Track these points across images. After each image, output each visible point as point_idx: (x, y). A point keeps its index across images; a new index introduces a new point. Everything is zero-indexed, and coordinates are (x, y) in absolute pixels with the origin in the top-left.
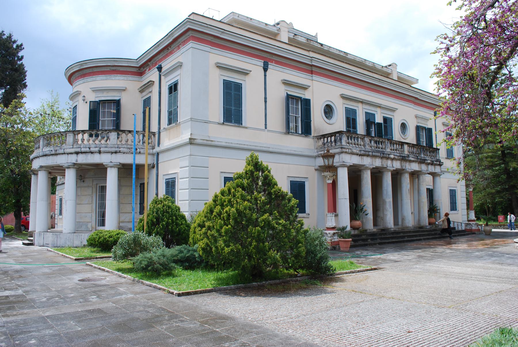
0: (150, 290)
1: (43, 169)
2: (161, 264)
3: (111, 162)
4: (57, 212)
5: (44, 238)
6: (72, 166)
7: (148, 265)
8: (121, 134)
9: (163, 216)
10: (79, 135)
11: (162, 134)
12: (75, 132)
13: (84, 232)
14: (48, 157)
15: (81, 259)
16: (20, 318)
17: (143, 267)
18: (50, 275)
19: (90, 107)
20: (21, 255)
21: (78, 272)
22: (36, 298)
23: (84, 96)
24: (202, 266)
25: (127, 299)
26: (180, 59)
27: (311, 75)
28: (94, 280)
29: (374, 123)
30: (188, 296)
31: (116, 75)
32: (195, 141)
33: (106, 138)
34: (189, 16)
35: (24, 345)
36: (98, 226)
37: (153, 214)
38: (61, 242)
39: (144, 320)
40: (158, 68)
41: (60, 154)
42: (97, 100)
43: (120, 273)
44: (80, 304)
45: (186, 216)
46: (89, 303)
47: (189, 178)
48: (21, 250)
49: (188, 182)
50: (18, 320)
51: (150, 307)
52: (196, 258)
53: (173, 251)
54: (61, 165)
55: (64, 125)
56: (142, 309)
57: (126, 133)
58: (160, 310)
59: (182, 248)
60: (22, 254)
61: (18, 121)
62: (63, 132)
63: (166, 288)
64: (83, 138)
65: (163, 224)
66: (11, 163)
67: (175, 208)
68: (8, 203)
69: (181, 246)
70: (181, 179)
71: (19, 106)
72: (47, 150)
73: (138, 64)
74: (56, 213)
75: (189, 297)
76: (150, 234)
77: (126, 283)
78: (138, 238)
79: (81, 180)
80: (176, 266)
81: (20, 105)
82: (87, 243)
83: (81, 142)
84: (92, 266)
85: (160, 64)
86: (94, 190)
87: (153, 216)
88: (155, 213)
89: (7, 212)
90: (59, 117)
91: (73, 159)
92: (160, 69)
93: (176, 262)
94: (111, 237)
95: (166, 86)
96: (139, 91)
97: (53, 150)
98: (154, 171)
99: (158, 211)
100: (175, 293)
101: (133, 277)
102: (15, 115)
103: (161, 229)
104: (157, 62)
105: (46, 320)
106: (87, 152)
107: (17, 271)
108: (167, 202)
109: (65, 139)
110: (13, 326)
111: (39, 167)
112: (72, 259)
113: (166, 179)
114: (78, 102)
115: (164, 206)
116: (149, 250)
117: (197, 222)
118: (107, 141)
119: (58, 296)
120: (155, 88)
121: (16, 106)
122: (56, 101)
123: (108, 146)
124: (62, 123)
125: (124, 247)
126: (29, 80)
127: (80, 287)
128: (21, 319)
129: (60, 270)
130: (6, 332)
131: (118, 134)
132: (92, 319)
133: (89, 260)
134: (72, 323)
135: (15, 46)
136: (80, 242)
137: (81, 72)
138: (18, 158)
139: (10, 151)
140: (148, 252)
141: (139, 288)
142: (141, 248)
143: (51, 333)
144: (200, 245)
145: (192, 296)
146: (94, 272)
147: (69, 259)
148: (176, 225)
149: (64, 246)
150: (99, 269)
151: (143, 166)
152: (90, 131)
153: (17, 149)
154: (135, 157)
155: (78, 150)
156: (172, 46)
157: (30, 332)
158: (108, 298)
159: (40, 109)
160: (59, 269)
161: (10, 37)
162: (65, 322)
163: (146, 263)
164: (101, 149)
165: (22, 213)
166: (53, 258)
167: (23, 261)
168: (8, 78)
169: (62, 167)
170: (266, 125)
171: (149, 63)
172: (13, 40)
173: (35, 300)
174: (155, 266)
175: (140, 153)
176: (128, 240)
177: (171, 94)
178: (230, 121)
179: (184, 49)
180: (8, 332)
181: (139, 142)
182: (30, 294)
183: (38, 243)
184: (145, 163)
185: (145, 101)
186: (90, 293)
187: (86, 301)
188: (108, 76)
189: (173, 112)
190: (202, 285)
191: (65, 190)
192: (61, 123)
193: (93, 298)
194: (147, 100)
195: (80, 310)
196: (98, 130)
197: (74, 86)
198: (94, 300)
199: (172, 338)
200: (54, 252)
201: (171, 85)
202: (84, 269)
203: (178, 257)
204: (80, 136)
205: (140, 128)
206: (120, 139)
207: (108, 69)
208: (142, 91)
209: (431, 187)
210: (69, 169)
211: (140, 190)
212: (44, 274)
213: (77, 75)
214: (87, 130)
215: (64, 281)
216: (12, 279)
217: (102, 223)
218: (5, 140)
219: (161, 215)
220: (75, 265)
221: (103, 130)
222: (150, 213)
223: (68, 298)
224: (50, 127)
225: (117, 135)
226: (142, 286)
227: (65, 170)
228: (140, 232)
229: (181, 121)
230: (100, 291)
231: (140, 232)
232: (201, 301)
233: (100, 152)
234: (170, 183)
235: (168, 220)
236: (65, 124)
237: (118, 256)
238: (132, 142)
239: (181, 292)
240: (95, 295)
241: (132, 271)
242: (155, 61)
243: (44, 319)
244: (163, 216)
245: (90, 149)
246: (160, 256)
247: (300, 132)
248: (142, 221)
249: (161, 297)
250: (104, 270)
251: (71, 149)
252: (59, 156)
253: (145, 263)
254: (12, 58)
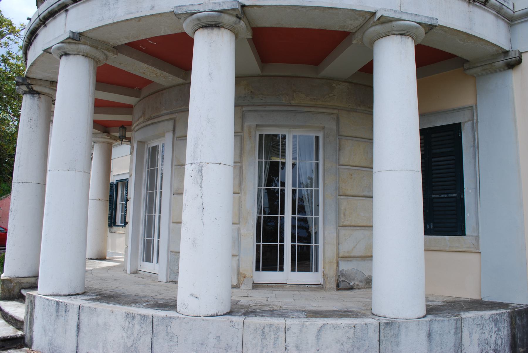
5: (83, 328)
183: (51, 344)
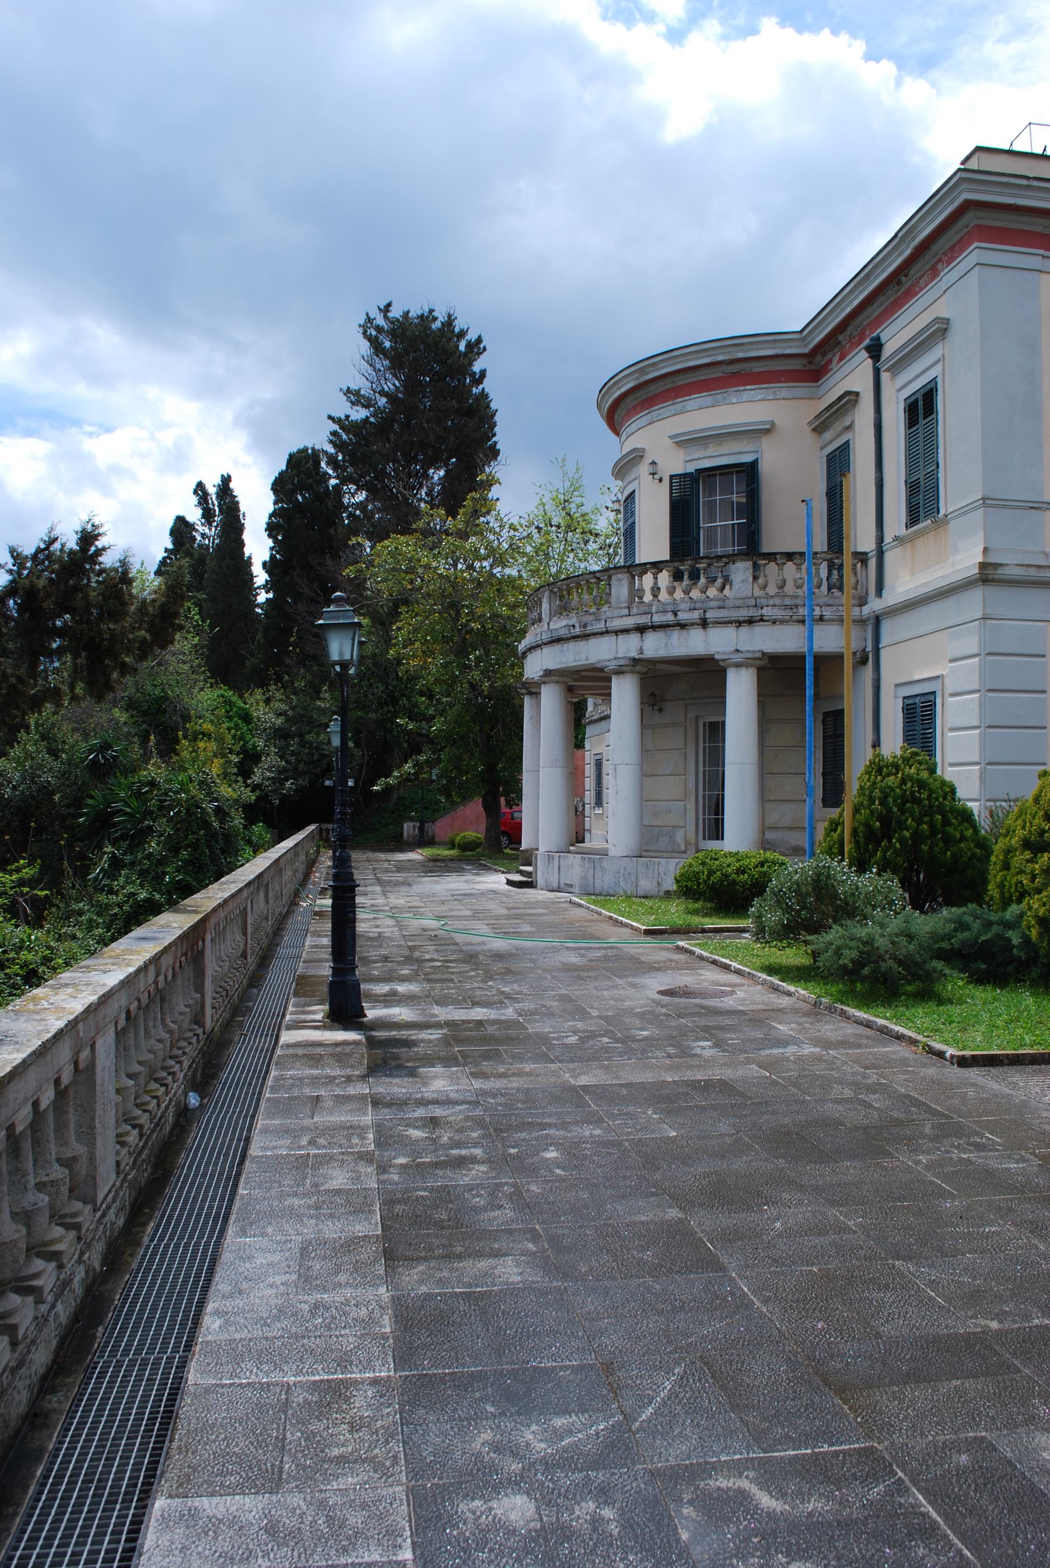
0: (868, 1038)
1: (553, 678)
2: (900, 963)
3: (737, 651)
4: (589, 797)
6: (630, 668)
7: (860, 962)
8: (765, 565)
9: (902, 811)
10: (644, 577)
11: (889, 557)
12: (634, 569)
13: (665, 855)
14: (566, 645)
15: (661, 932)
16: (515, 1083)
17: (844, 966)
18: (584, 970)
19: (671, 493)
20: (504, 912)
21: (658, 969)
22: (550, 1033)
23: (654, 463)
24: (1034, 975)
25: (801, 1059)
26: (942, 310)
28: (703, 994)
30: (991, 1069)
31: (742, 388)
32: (999, 572)
33: (720, 581)
34: (963, 163)
35: (529, 1161)
36: (704, 839)
37: (869, 806)
38: (604, 881)
39: (857, 1128)
40: (868, 349)
41: (595, 634)
42: (691, 468)
43: (775, 980)
44: (667, 1061)
45: (976, 812)
46: (694, 1062)
47: (978, 691)
48: (505, 900)
49: (976, 705)
50: (511, 1089)
51: (875, 1092)
52: (1013, 947)
53: (935, 922)
54: (598, 666)
55: (600, 552)
56: (848, 1093)
57: (780, 561)
58: (904, 1103)
59: (965, 913)
60: (509, 909)
61: (482, 551)
62: (599, 571)
63: (920, 1038)
64: (656, 583)
65: (904, 836)
66: (469, 667)
67: (941, 788)
68: (467, 773)
69: (964, 909)
70: (952, 695)
71: (484, 510)
72: (560, 625)
73: (806, 346)
74: (587, 800)
75: (994, 1071)
76: (862, 867)
77: (796, 1011)
78: (828, 877)
79: (653, 705)
80: (947, 971)
81: (484, 506)
82: (675, 887)
83: (651, 598)
84: (692, 953)
85: (875, 334)
86: (691, 734)
87: (872, 812)
88: (877, 802)
89: (465, 798)
90: (586, 530)
91: (629, 647)
92: (875, 350)
93: (947, 956)
94: (744, 872)
95: (897, 403)
96: (814, 430)
97: (577, 625)
98: (868, 671)
99: (886, 796)
100: (948, 1055)
101: (815, 994)
102: (475, 534)
103: (896, 852)
104: (865, 329)
105: (583, 1097)
106: (669, 626)
107: (499, 956)
108: (913, 770)
109: (607, 590)
110: (500, 1105)
111: (541, 673)
112: (636, 929)
113: (904, 698)
114: (636, 482)
115: (903, 781)
116: (861, 915)
117: (1020, 833)
118: (722, 589)
119: (608, 1033)
120: (863, 416)
121: (476, 511)
122: (576, 487)
123: (727, 603)
124: (595, 546)
125: (787, 904)
126: (502, 437)
127: (664, 1010)
128: (518, 1089)
129: (606, 958)
130: (484, 1120)
131: (756, 567)
132: (703, 1108)
133: (683, 936)
134: (650, 1113)
135: (462, 347)
136: (655, 883)
137: (640, 393)
138: (487, 652)
139: (467, 633)
140: (858, 922)
141: (831, 1029)
142: (837, 909)
143: (598, 1136)
144: (1030, 908)
145: (1006, 1068)
146: (700, 971)
147: (628, 930)
148: (944, 842)
149: (612, 892)
150: (714, 962)
151: (837, 659)
152: (676, 564)
153: (483, 627)
154: (811, 632)
155: (644, 620)
156: (911, 273)
157: (543, 1126)
158: (746, 1052)
159: (536, 512)
160: (605, 956)
161: (450, 322)
162: (631, 1109)
163: (855, 954)
164: (708, 615)
165: (502, 800)
166: (585, 924)
167: (511, 930)
168: (452, 438)
169: (601, 670)
171: (841, 337)
172: (457, 330)
173: (548, 1038)
174: (883, 964)
175: (821, 619)
176: (797, 883)
177: (916, 427)
179: (955, 274)
180: (488, 1119)
181: (819, 586)
182: (537, 1021)
184: (844, 650)
185: (831, 459)
186: (692, 1031)
187: (685, 1052)
188: (719, 395)
189: (922, 484)
190: (1037, 1035)
191: (611, 737)
192: (592, 546)
193: (703, 1048)
194: (837, 453)
195: (670, 1079)
196: (698, 559)
197: (624, 437)
198: (708, 1053)
199: (953, 1197)
200: (588, 908)
201: (912, 399)
202: (671, 961)
203: (953, 941)
204: (648, 580)
205: (820, 543)
206: (761, 580)
207: (716, 373)
208: (820, 426)
210: (621, 676)
211: (824, 733)
212: (568, 968)
213: (629, 401)
214: (666, 561)
215: (621, 992)
216: (489, 976)
217: (716, 830)
218: (455, 605)
219: (895, 809)
220: (646, 948)
221: (712, 558)
222: (861, 804)
223: (635, 1040)
224: (563, 561)
225: (751, 570)
226: (843, 1024)
227: (609, 680)
228: (833, 859)
229: (950, 510)
230: (720, 1028)
231: (833, 859)
232: (1037, 1089)
233: (704, 623)
234: (919, 710)
235: (919, 822)
236: (601, 548)
237: (770, 928)
238: (798, 587)
239: (968, 1053)
240: (707, 1040)
241: (809, 975)
242: (859, 329)
243: (574, 1094)
244: (903, 811)
245: (676, 615)
246: (897, 935)
248: (837, 824)
249: (905, 1062)
250: (726, 968)
251: (625, 618)
252: (593, 641)
253: (853, 956)
254: (459, 380)
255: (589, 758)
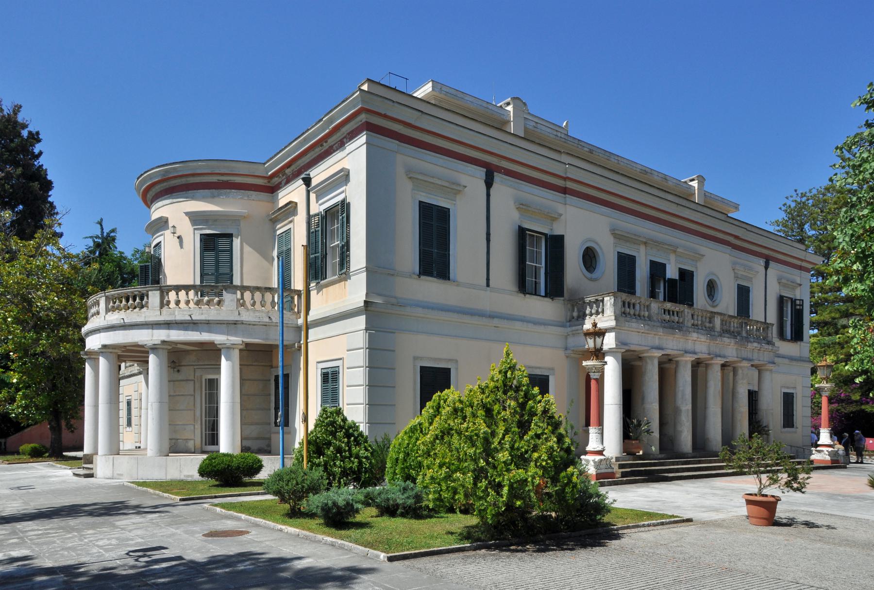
4: (123, 421)
23: (174, 227)
26: (346, 164)
27: (563, 195)
29: (665, 279)
36: (206, 445)
72: (115, 318)
79: (174, 368)
91: (160, 335)
92: (307, 181)
111: (100, 347)
114: (163, 236)
169: (142, 346)
170: (488, 279)
178: (430, 274)
194: (284, 234)
204: (182, 293)
209: (756, 389)
217: (214, 439)
247: (543, 293)
255: (123, 399)
